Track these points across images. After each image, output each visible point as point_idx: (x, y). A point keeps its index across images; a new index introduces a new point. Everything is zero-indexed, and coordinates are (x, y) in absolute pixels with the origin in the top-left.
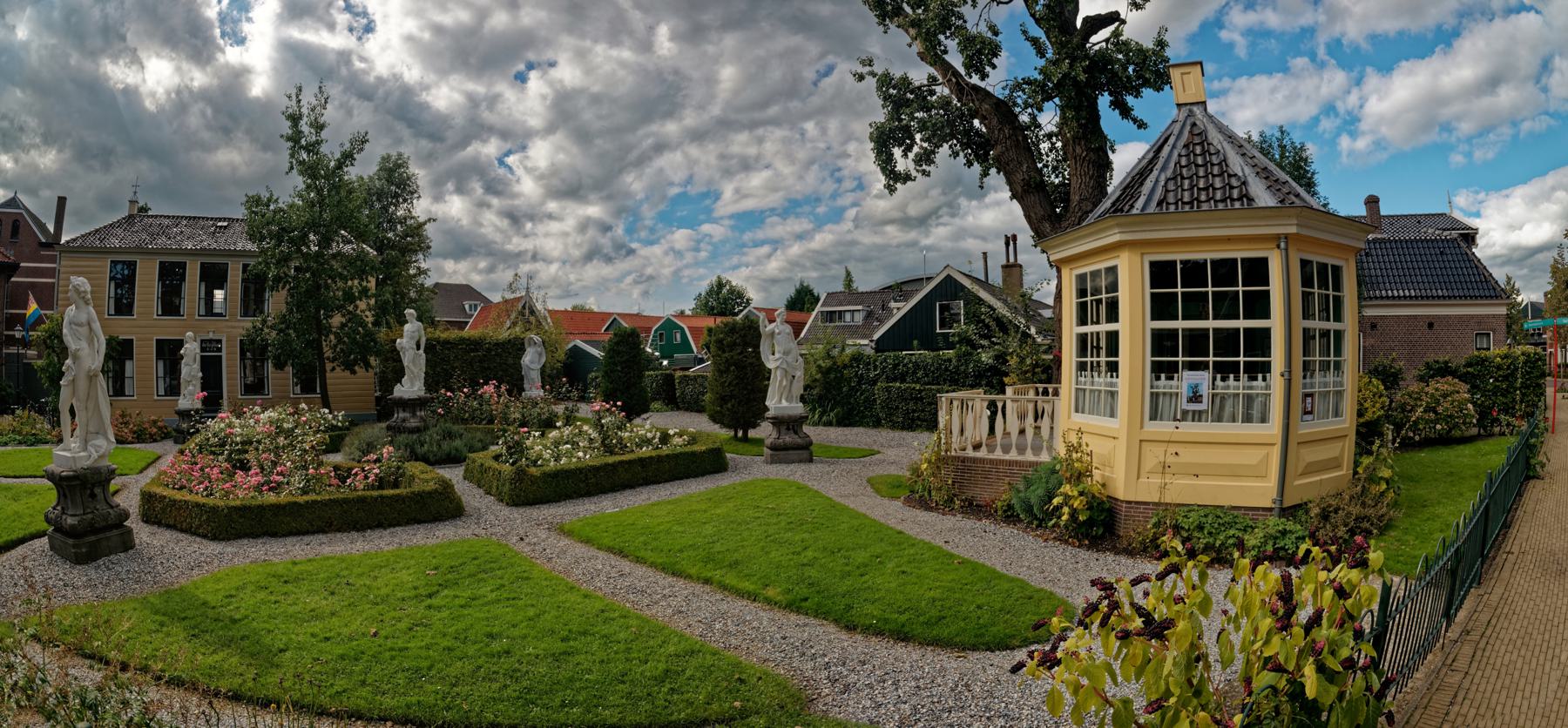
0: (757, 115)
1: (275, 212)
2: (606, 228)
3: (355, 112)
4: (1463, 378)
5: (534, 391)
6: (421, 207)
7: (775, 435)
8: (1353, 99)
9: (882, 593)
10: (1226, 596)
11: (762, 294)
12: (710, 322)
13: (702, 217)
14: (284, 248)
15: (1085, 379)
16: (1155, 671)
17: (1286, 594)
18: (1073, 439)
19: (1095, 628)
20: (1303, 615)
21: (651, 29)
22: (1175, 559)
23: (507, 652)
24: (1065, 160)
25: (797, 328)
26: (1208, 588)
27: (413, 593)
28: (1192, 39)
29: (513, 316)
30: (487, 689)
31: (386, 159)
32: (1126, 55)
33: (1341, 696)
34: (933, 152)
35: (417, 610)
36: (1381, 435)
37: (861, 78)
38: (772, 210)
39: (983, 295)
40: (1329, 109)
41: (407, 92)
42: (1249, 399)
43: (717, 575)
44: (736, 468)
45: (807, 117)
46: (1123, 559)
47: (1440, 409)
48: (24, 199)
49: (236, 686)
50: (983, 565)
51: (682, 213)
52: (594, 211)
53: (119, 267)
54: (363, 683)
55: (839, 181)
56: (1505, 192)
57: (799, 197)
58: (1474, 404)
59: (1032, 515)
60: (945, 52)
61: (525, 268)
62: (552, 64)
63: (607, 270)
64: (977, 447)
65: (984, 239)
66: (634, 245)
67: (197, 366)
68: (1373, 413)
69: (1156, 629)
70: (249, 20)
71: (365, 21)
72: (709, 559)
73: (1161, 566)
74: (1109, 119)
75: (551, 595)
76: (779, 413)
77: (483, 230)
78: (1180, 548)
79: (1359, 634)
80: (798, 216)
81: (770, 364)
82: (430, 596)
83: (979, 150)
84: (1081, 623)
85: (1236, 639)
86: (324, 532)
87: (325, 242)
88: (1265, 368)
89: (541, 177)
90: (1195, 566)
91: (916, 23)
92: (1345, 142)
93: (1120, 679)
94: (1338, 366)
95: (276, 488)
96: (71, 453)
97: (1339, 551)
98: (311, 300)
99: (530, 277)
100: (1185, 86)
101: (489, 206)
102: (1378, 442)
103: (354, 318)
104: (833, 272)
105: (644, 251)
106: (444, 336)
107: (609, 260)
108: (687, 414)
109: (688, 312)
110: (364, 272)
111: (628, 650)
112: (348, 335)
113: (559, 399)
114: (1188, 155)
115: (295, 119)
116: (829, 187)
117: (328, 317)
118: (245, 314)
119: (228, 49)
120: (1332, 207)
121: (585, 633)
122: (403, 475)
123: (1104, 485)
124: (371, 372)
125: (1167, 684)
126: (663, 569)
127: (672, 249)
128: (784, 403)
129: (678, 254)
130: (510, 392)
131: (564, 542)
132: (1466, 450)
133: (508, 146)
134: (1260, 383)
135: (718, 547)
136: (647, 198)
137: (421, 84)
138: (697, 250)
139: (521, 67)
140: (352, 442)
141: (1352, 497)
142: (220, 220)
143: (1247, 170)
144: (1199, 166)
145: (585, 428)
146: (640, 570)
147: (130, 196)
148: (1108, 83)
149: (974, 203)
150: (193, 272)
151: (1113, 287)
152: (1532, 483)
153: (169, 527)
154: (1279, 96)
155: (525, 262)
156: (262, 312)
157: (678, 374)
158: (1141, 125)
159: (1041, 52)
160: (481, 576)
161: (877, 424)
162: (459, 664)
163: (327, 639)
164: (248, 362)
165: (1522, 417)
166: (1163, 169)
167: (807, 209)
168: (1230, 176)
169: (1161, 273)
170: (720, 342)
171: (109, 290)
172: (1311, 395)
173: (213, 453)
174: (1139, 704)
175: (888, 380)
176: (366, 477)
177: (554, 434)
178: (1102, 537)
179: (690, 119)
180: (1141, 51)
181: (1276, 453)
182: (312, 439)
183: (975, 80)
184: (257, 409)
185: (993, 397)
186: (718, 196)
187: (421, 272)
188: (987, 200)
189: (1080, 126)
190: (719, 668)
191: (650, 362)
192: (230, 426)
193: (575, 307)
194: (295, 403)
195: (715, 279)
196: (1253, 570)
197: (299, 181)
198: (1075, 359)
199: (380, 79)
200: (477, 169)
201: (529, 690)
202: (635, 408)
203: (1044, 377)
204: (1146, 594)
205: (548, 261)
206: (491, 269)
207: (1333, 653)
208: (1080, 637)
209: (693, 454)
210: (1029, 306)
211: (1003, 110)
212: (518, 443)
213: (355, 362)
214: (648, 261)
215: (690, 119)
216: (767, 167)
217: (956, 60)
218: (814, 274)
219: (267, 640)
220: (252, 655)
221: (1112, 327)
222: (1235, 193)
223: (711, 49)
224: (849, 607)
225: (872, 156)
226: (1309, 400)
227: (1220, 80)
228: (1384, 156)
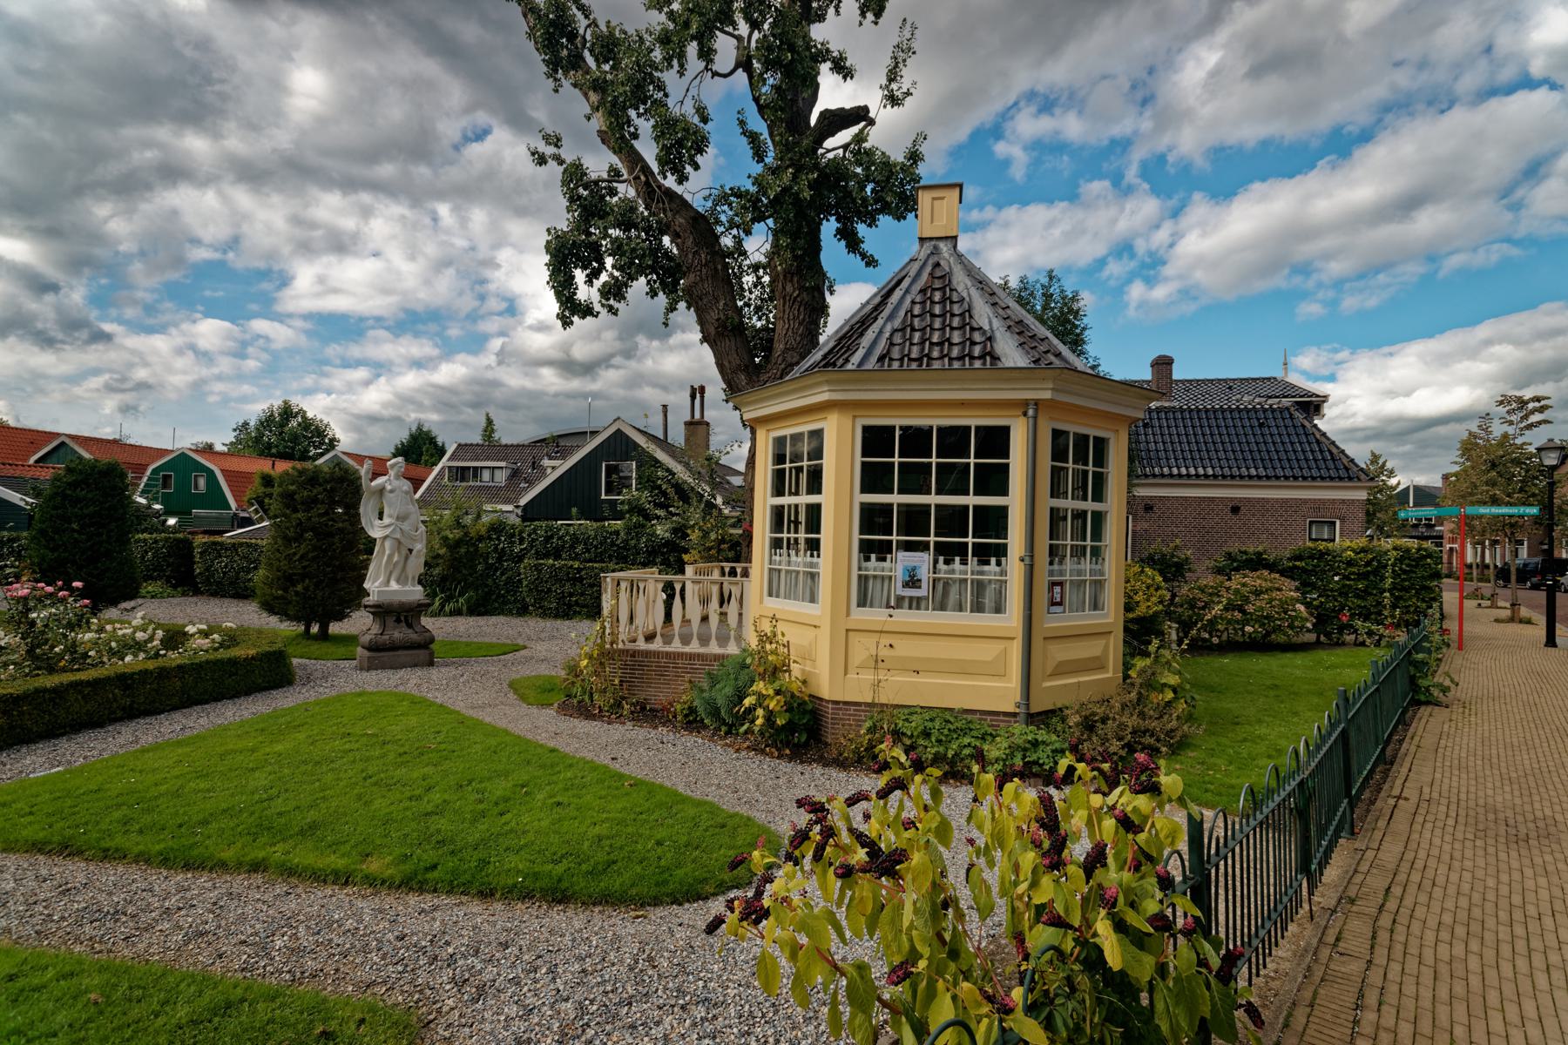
2: (41, 286)
4: (1287, 573)
7: (376, 629)
8: (1162, 236)
9: (531, 836)
10: (969, 820)
11: (355, 436)
12: (263, 466)
13: (254, 307)
15: (781, 559)
16: (893, 922)
17: (1049, 820)
18: (767, 627)
19: (807, 863)
20: (1079, 850)
22: (899, 773)
24: (771, 299)
26: (944, 809)
28: (957, 152)
32: (867, 169)
33: (1162, 970)
36: (1160, 634)
38: (379, 319)
39: (661, 455)
40: (1124, 249)
42: (980, 587)
43: (277, 853)
45: (441, 195)
46: (834, 772)
47: (1250, 608)
50: (661, 786)
56: (1386, 350)
57: (420, 308)
58: (1308, 605)
59: (719, 719)
60: (635, 136)
63: (43, 360)
64: (650, 638)
65: (665, 388)
66: (108, 327)
68: (1147, 606)
69: (886, 864)
72: (264, 828)
73: (882, 781)
74: (832, 251)
76: (386, 599)
78: (903, 758)
79: (1166, 883)
80: (417, 335)
83: (667, 277)
84: (789, 857)
85: (992, 877)
88: (1001, 552)
90: (924, 781)
91: (599, 86)
92: (1137, 291)
93: (848, 934)
94: (1096, 552)
97: (1114, 769)
100: (934, 214)
102: (1156, 643)
104: (462, 417)
107: (46, 341)
109: (219, 448)
114: (923, 303)
120: (1104, 369)
123: (804, 682)
125: (911, 940)
127: (193, 347)
128: (394, 586)
129: (204, 357)
132: (1299, 660)
134: (993, 567)
135: (278, 805)
136: (142, 254)
138: (240, 354)
141: (1124, 706)
143: (996, 323)
144: (935, 317)
146: (110, 874)
148: (837, 205)
149: (655, 343)
151: (817, 453)
152: (1424, 711)
154: (1057, 232)
157: (201, 539)
158: (871, 262)
159: (759, 155)
161: (523, 611)
165: (1398, 626)
166: (891, 318)
168: (973, 329)
169: (876, 440)
170: (288, 498)
172: (1061, 584)
174: (879, 970)
175: (538, 555)
178: (806, 745)
179: (235, 143)
180: (887, 165)
181: (1016, 650)
183: (670, 182)
185: (670, 577)
186: (285, 281)
188: (672, 341)
189: (795, 258)
190: (285, 1024)
195: (277, 403)
196: (1000, 788)
198: (768, 535)
202: (110, 590)
203: (731, 554)
204: (867, 817)
207: (1132, 905)
208: (790, 877)
209: (233, 662)
210: (716, 472)
211: (701, 227)
216: (376, 255)
217: (648, 150)
221: (813, 499)
222: (977, 351)
224: (484, 863)
226: (1057, 589)
227: (981, 208)
228: (1191, 308)
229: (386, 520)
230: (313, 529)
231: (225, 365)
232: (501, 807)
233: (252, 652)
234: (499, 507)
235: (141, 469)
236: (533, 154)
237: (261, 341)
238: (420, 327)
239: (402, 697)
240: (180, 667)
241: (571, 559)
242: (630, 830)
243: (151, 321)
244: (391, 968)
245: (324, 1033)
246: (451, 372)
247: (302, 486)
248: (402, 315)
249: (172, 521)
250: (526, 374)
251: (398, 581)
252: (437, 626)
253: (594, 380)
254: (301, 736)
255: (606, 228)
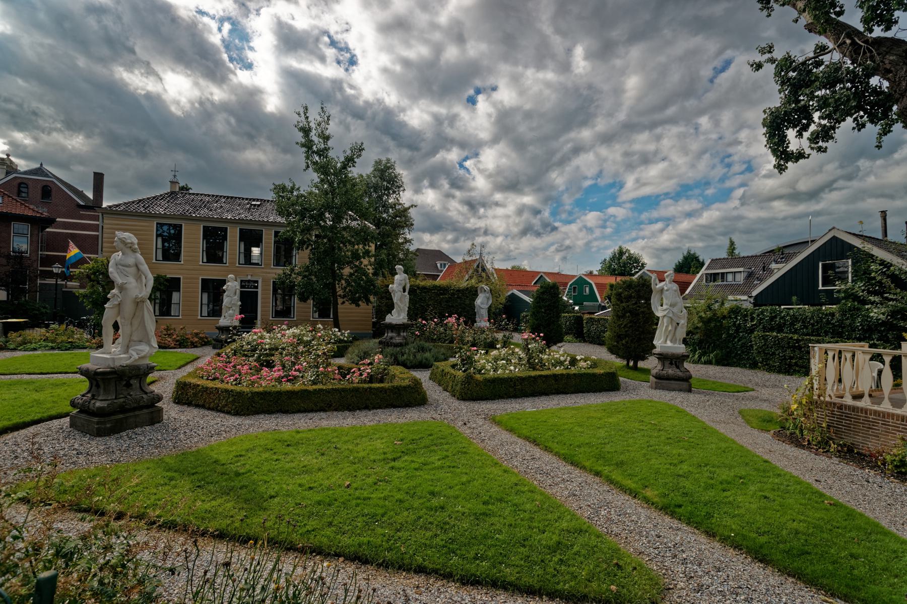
0: (657, 117)
1: (297, 196)
2: (536, 212)
3: (352, 128)
5: (483, 322)
6: (406, 197)
7: (659, 367)
9: (742, 511)
11: (655, 260)
12: (612, 280)
13: (609, 202)
14: (307, 221)
21: (569, 51)
23: (442, 508)
25: (683, 286)
27: (382, 456)
29: (470, 272)
30: (422, 536)
31: (378, 162)
34: (833, 128)
35: (382, 470)
37: (759, 66)
41: (389, 113)
43: (606, 470)
44: (626, 390)
45: (701, 112)
48: (48, 168)
49: (224, 526)
51: (593, 199)
52: (528, 199)
53: (165, 228)
54: (330, 524)
55: (729, 166)
61: (479, 240)
62: (494, 89)
64: (858, 397)
66: (557, 224)
67: (237, 297)
70: (251, 49)
71: (348, 55)
72: (600, 457)
75: (480, 467)
76: (664, 351)
77: (450, 214)
80: (688, 198)
81: (659, 312)
82: (394, 460)
86: (324, 410)
87: (338, 218)
89: (489, 176)
95: (293, 380)
96: (111, 354)
98: (328, 256)
99: (483, 246)
101: (453, 197)
103: (359, 270)
104: (716, 243)
105: (564, 229)
106: (422, 284)
107: (538, 234)
108: (591, 346)
109: (595, 273)
110: (366, 240)
111: (531, 519)
112: (355, 281)
113: (500, 329)
115: (306, 131)
116: (720, 171)
117: (340, 268)
118: (277, 264)
119: (238, 72)
121: (501, 500)
122: (387, 374)
124: (370, 306)
126: (565, 458)
127: (585, 227)
128: (669, 344)
129: (590, 230)
130: (466, 323)
131: (495, 429)
133: (465, 154)
135: (608, 448)
136: (567, 189)
137: (398, 107)
138: (604, 227)
139: (471, 92)
140: (353, 351)
142: (254, 200)
145: (517, 350)
146: (547, 457)
147: (171, 178)
150: (233, 235)
153: (197, 406)
155: (479, 236)
156: (290, 263)
157: (586, 316)
160: (432, 448)
161: (754, 366)
162: (406, 513)
163: (311, 488)
164: (279, 297)
167: (697, 191)
170: (619, 295)
171: (155, 244)
173: (246, 356)
175: (765, 329)
176: (361, 375)
177: (494, 353)
179: (601, 125)
182: (324, 348)
184: (284, 327)
186: (621, 185)
187: (407, 241)
190: (601, 550)
191: (565, 307)
192: (261, 337)
193: (513, 267)
194: (314, 324)
195: (617, 248)
197: (315, 177)
199: (367, 102)
200: (444, 170)
201: (453, 541)
202: (552, 339)
205: (495, 235)
206: (456, 240)
209: (594, 375)
212: (469, 358)
213: (359, 299)
214: (566, 236)
215: (601, 125)
218: (700, 244)
219: (262, 489)
220: (246, 501)
223: (618, 62)
225: (764, 140)
229: (665, 307)
230: (630, 312)
231: (598, 233)
232: (724, 486)
233: (602, 371)
234: (739, 297)
235: (565, 284)
236: (752, 66)
237: (612, 218)
238: (690, 193)
239: (671, 407)
240: (574, 374)
241: (793, 333)
242: (825, 535)
243: (571, 218)
244: (652, 550)
245: (617, 564)
246: (710, 216)
247: (625, 289)
248: (679, 189)
249: (577, 308)
250: (762, 208)
251: (671, 341)
252: (693, 369)
253: (818, 202)
254: (621, 417)
255: (812, 93)
